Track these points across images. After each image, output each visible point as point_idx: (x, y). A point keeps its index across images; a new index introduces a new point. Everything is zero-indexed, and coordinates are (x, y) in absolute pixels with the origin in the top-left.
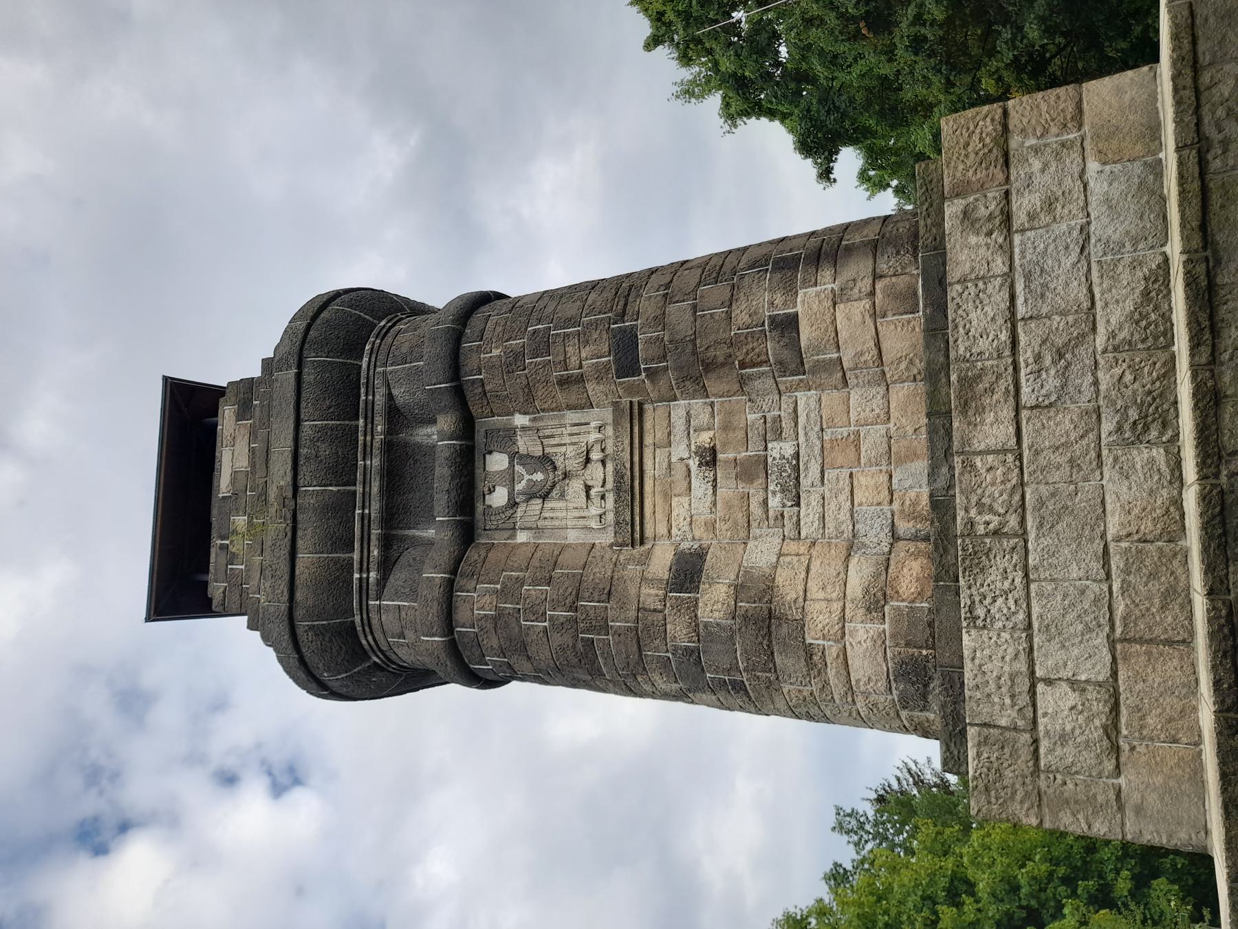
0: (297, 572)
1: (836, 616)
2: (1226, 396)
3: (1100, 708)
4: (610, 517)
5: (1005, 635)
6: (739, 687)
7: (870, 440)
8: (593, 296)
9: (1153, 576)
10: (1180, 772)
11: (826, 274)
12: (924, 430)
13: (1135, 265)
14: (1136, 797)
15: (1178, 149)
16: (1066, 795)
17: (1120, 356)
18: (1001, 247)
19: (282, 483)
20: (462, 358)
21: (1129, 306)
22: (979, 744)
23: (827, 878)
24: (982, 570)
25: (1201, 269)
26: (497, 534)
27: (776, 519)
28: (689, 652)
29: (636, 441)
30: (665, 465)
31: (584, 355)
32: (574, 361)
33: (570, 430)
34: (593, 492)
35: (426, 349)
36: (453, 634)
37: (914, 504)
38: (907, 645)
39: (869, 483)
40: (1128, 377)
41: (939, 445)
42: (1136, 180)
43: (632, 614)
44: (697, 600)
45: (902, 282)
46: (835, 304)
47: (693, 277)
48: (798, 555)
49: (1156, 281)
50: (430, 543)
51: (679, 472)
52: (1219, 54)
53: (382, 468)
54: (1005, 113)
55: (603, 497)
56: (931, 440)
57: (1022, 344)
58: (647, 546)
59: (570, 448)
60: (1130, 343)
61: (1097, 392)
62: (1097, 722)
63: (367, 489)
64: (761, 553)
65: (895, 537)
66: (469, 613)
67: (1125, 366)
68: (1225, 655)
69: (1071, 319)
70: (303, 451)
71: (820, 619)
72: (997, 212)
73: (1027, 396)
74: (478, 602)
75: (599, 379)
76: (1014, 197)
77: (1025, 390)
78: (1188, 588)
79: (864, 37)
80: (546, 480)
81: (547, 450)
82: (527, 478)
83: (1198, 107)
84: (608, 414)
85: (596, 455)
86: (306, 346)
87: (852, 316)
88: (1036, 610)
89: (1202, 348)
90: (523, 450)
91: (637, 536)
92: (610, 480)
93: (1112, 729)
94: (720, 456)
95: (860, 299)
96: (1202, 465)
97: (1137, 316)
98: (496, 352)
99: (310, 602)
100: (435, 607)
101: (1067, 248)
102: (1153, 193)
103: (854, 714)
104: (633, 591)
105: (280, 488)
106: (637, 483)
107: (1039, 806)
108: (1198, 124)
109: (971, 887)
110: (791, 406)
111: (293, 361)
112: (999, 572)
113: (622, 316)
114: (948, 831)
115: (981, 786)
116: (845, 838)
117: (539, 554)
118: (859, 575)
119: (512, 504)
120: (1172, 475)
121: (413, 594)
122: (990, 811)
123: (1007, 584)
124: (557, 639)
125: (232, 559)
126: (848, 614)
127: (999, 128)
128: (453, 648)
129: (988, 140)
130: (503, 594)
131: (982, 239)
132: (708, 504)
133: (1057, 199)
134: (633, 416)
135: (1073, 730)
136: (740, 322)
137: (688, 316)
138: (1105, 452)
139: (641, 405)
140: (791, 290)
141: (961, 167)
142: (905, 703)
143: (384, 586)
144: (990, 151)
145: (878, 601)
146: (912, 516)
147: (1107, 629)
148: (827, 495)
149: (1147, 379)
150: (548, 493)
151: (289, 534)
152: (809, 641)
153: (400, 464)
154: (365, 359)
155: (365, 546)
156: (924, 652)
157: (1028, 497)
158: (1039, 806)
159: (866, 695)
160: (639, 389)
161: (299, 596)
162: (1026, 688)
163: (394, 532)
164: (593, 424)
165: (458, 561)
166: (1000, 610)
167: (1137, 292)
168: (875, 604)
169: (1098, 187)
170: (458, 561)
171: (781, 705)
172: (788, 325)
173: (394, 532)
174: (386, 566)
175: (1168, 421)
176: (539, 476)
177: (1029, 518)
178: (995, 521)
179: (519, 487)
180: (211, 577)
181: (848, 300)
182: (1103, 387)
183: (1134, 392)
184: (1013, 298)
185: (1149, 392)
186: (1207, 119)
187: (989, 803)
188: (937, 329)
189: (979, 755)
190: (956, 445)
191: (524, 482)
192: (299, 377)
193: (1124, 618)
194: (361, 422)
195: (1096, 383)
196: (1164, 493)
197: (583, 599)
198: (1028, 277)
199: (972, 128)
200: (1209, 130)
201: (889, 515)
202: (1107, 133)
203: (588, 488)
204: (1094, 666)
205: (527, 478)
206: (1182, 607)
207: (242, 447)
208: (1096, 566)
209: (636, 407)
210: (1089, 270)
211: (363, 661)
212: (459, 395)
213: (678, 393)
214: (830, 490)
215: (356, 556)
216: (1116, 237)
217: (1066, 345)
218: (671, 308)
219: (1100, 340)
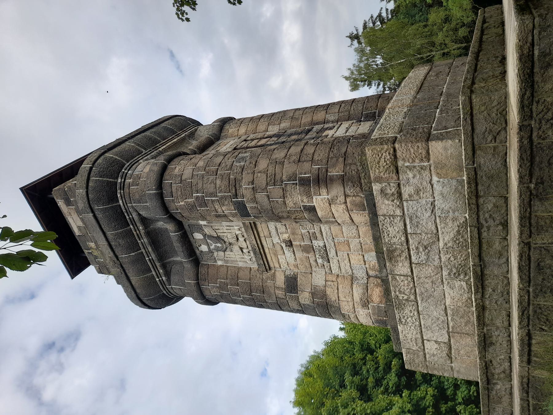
1: (351, 306)
4: (254, 259)
5: (413, 328)
11: (324, 191)
18: (398, 206)
20: (167, 204)
21: (452, 235)
24: (403, 309)
25: (478, 269)
41: (382, 262)
42: (454, 187)
45: (358, 199)
46: (330, 204)
48: (333, 281)
49: (462, 227)
52: (487, 192)
53: (149, 242)
57: (410, 242)
58: (273, 271)
61: (441, 261)
65: (369, 277)
67: (451, 255)
68: (484, 373)
70: (113, 244)
72: (395, 193)
77: (413, 258)
81: (219, 234)
83: (478, 211)
86: (91, 203)
91: (268, 268)
92: (249, 246)
94: (293, 243)
97: (455, 239)
98: (183, 203)
101: (426, 210)
104: (272, 292)
106: (262, 251)
110: (319, 229)
112: (408, 310)
118: (358, 292)
127: (393, 157)
129: (388, 162)
130: (220, 288)
131: (390, 202)
133: (420, 190)
137: (266, 199)
138: (444, 280)
141: (377, 171)
144: (390, 167)
145: (366, 304)
148: (340, 260)
151: (123, 273)
153: (156, 239)
157: (417, 291)
161: (138, 291)
168: (365, 304)
169: (438, 188)
174: (168, 274)
178: (406, 297)
182: (443, 260)
184: (405, 225)
185: (460, 264)
195: (440, 258)
196: (466, 295)
198: (411, 219)
199: (380, 155)
202: (440, 166)
203: (241, 249)
207: (75, 216)
208: (443, 313)
209: (253, 224)
216: (446, 208)
218: (258, 195)
219: (441, 244)
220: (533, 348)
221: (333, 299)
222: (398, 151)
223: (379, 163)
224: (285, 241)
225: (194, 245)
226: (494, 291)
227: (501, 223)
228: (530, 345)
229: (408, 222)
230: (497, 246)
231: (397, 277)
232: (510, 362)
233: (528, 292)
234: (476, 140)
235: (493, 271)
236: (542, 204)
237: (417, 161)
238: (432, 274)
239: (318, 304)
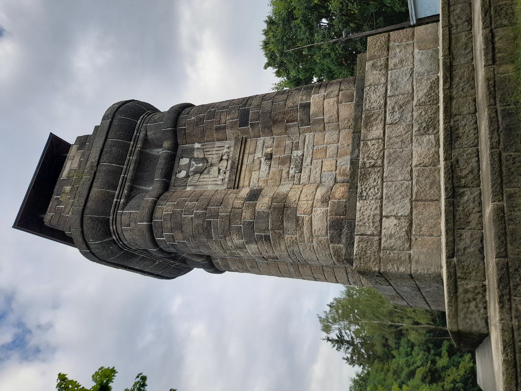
0: (90, 195)
2: (454, 98)
3: (405, 224)
4: (226, 180)
7: (330, 150)
9: (427, 177)
10: (432, 246)
12: (350, 145)
14: (416, 257)
15: (442, 27)
16: (390, 258)
17: (421, 107)
21: (425, 91)
22: (359, 242)
24: (367, 180)
25: (448, 61)
27: (292, 177)
28: (250, 223)
29: (242, 151)
30: (252, 160)
31: (227, 118)
32: (223, 121)
33: (216, 149)
36: (152, 222)
37: (344, 170)
38: (336, 214)
39: (328, 164)
40: (423, 113)
42: (430, 54)
43: (229, 210)
44: (256, 203)
45: (348, 92)
51: (257, 162)
54: (389, 36)
55: (225, 173)
60: (424, 103)
61: (413, 119)
62: (404, 230)
63: (128, 168)
65: (336, 182)
66: (161, 213)
69: (405, 96)
70: (105, 149)
71: (304, 206)
73: (388, 120)
75: (232, 128)
77: (388, 118)
78: (439, 181)
80: (203, 166)
82: (195, 165)
84: (232, 142)
85: (225, 157)
87: (330, 104)
89: (447, 84)
91: (236, 185)
93: (409, 232)
94: (274, 157)
95: (333, 97)
96: (445, 119)
97: (427, 94)
98: (193, 118)
99: (93, 207)
100: (147, 210)
101: (406, 74)
102: (435, 58)
103: (312, 248)
105: (92, 163)
106: (239, 166)
107: (379, 263)
108: (449, 20)
112: (373, 179)
115: (358, 257)
119: (187, 176)
120: (436, 143)
122: (360, 266)
124: (196, 222)
125: (60, 203)
127: (387, 39)
132: (266, 173)
135: (395, 233)
136: (289, 106)
137: (270, 104)
138: (414, 138)
139: (246, 139)
140: (309, 95)
143: (126, 206)
146: (344, 175)
147: (410, 197)
149: (429, 114)
150: (203, 171)
151: (91, 180)
152: (298, 215)
153: (143, 163)
154: (139, 121)
155: (122, 189)
156: (342, 217)
158: (379, 263)
161: (89, 204)
162: (378, 219)
163: (135, 186)
165: (160, 195)
166: (372, 193)
167: (428, 87)
168: (325, 201)
169: (417, 57)
170: (160, 195)
173: (135, 186)
175: (435, 127)
178: (373, 162)
179: (191, 169)
181: (329, 98)
182: (414, 117)
183: (425, 118)
184: (386, 90)
185: (430, 118)
187: (361, 263)
189: (358, 246)
190: (362, 138)
192: (111, 123)
193: (416, 193)
194: (132, 142)
195: (412, 116)
198: (392, 84)
200: (452, 22)
201: (335, 175)
203: (219, 170)
204: (404, 210)
205: (195, 165)
206: (437, 188)
207: (77, 160)
208: (408, 176)
210: (413, 81)
211: (109, 237)
212: (175, 133)
213: (261, 133)
214: (314, 167)
215: (117, 192)
216: (422, 71)
217: (403, 104)
219: (415, 102)
220: (497, 45)
226: (460, 79)
227: (466, 21)
228: (493, 43)
229: (389, 87)
230: (464, 40)
231: (369, 143)
232: (478, 156)
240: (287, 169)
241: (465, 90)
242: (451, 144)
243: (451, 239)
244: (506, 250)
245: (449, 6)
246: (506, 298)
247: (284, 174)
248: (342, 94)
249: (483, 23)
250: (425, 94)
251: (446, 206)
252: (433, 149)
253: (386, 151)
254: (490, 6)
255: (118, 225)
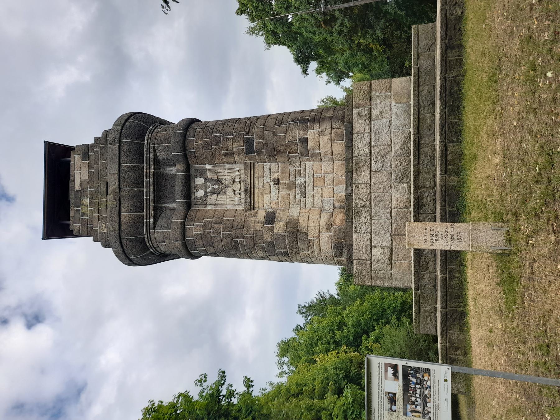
0: (122, 220)
1: (317, 231)
3: (388, 253)
4: (243, 201)
5: (365, 235)
6: (286, 254)
8: (236, 126)
9: (402, 218)
11: (317, 126)
13: (403, 133)
14: (396, 275)
19: (114, 187)
20: (187, 143)
23: (294, 330)
25: (417, 139)
26: (199, 206)
29: (252, 176)
31: (234, 146)
32: (230, 147)
33: (227, 171)
34: (236, 192)
35: (173, 139)
37: (340, 198)
39: (327, 191)
40: (399, 164)
43: (252, 232)
47: (272, 122)
50: (174, 209)
51: (267, 186)
54: (371, 84)
55: (240, 194)
56: (346, 179)
58: (256, 210)
59: (227, 177)
62: (387, 257)
64: (294, 212)
65: (334, 207)
70: (122, 175)
71: (312, 232)
74: (195, 229)
75: (239, 155)
76: (372, 110)
77: (373, 166)
79: (322, 27)
80: (219, 188)
81: (219, 177)
82: (211, 187)
84: (242, 166)
85: (237, 180)
86: (122, 135)
87: (324, 140)
88: (373, 228)
90: (209, 177)
91: (252, 207)
93: (390, 258)
94: (281, 182)
96: (414, 190)
98: (200, 142)
104: (252, 225)
106: (252, 189)
108: (418, 101)
109: (345, 325)
111: (117, 141)
112: (364, 217)
113: (248, 133)
114: (338, 308)
116: (301, 316)
117: (217, 213)
119: (206, 196)
121: (169, 227)
123: (366, 221)
124: (225, 241)
125: (83, 214)
126: (321, 231)
128: (185, 245)
130: (205, 226)
131: (363, 122)
132: (277, 197)
134: (251, 167)
137: (272, 135)
139: (253, 163)
140: (306, 130)
142: (336, 255)
146: (340, 201)
151: (118, 206)
153: (161, 181)
154: (146, 142)
159: (325, 253)
160: (254, 158)
161: (123, 228)
164: (236, 169)
168: (329, 227)
169: (394, 110)
171: (299, 258)
172: (305, 141)
174: (157, 217)
176: (216, 186)
177: (372, 202)
178: (363, 203)
179: (208, 190)
180: (70, 222)
184: (371, 139)
186: (420, 99)
188: (349, 147)
191: (210, 188)
192: (119, 147)
194: (145, 165)
195: (391, 165)
197: (234, 228)
198: (375, 134)
200: (421, 103)
202: (398, 94)
203: (234, 191)
205: (211, 187)
208: (389, 215)
211: (147, 251)
212: (185, 157)
215: (145, 213)
216: (398, 125)
218: (266, 132)
220: (449, 158)
221: (304, 225)
222: (373, 85)
223: (360, 92)
224: (274, 180)
225: (193, 189)
226: (425, 157)
228: (446, 156)
229: (373, 137)
230: (428, 121)
231: (359, 186)
233: (445, 112)
234: (420, 50)
235: (426, 140)
236: (452, 52)
237: (384, 91)
238: (385, 180)
239: (289, 232)
240: (294, 195)
241: (428, 167)
242: (418, 210)
243: (417, 279)
244: (446, 304)
245: (419, 86)
246: (444, 332)
247: (292, 199)
248: (334, 133)
249: (440, 137)
250: (400, 148)
251: (414, 256)
252: (406, 196)
253: (372, 195)
254: (446, 122)
255: (154, 242)
